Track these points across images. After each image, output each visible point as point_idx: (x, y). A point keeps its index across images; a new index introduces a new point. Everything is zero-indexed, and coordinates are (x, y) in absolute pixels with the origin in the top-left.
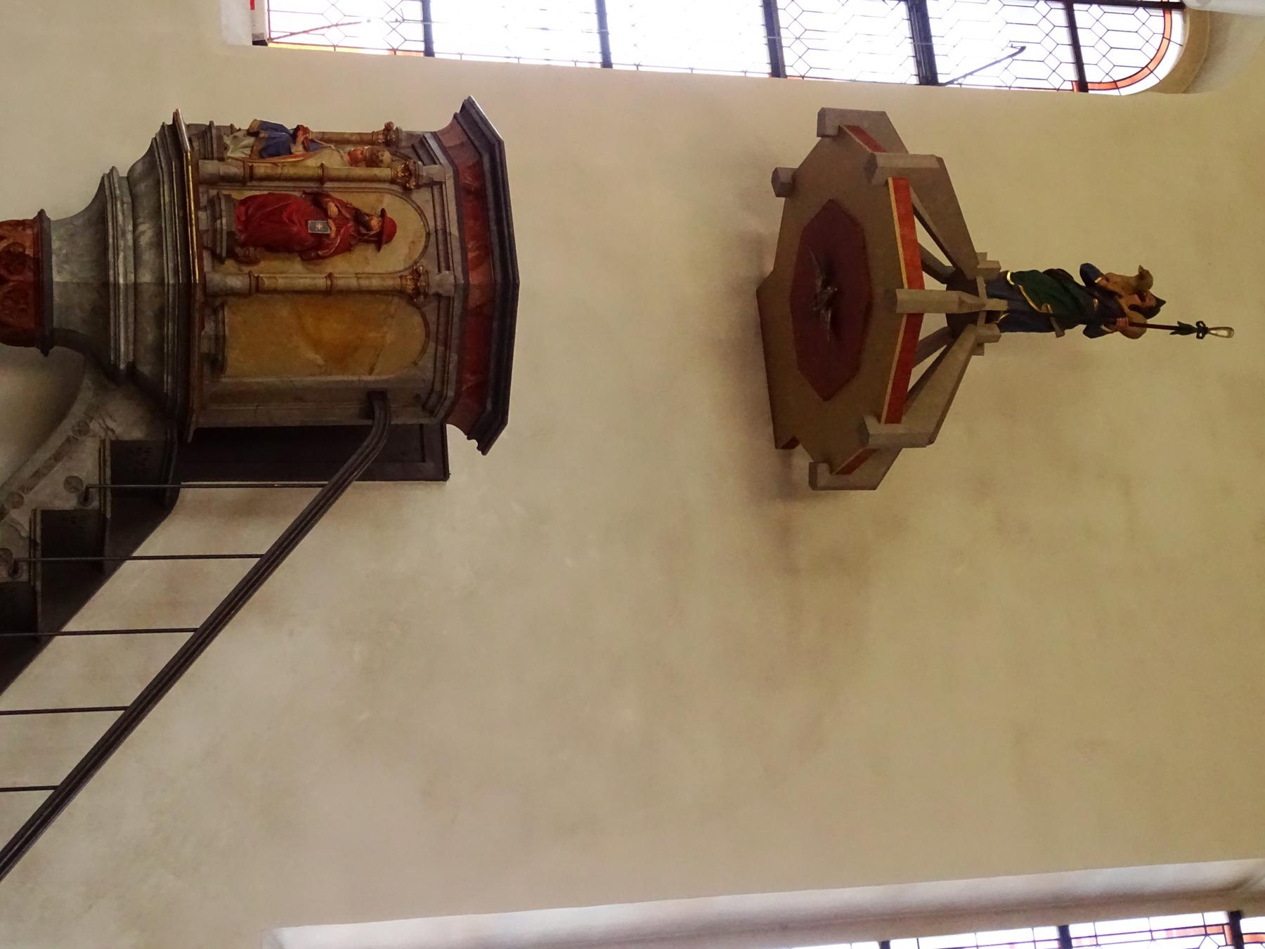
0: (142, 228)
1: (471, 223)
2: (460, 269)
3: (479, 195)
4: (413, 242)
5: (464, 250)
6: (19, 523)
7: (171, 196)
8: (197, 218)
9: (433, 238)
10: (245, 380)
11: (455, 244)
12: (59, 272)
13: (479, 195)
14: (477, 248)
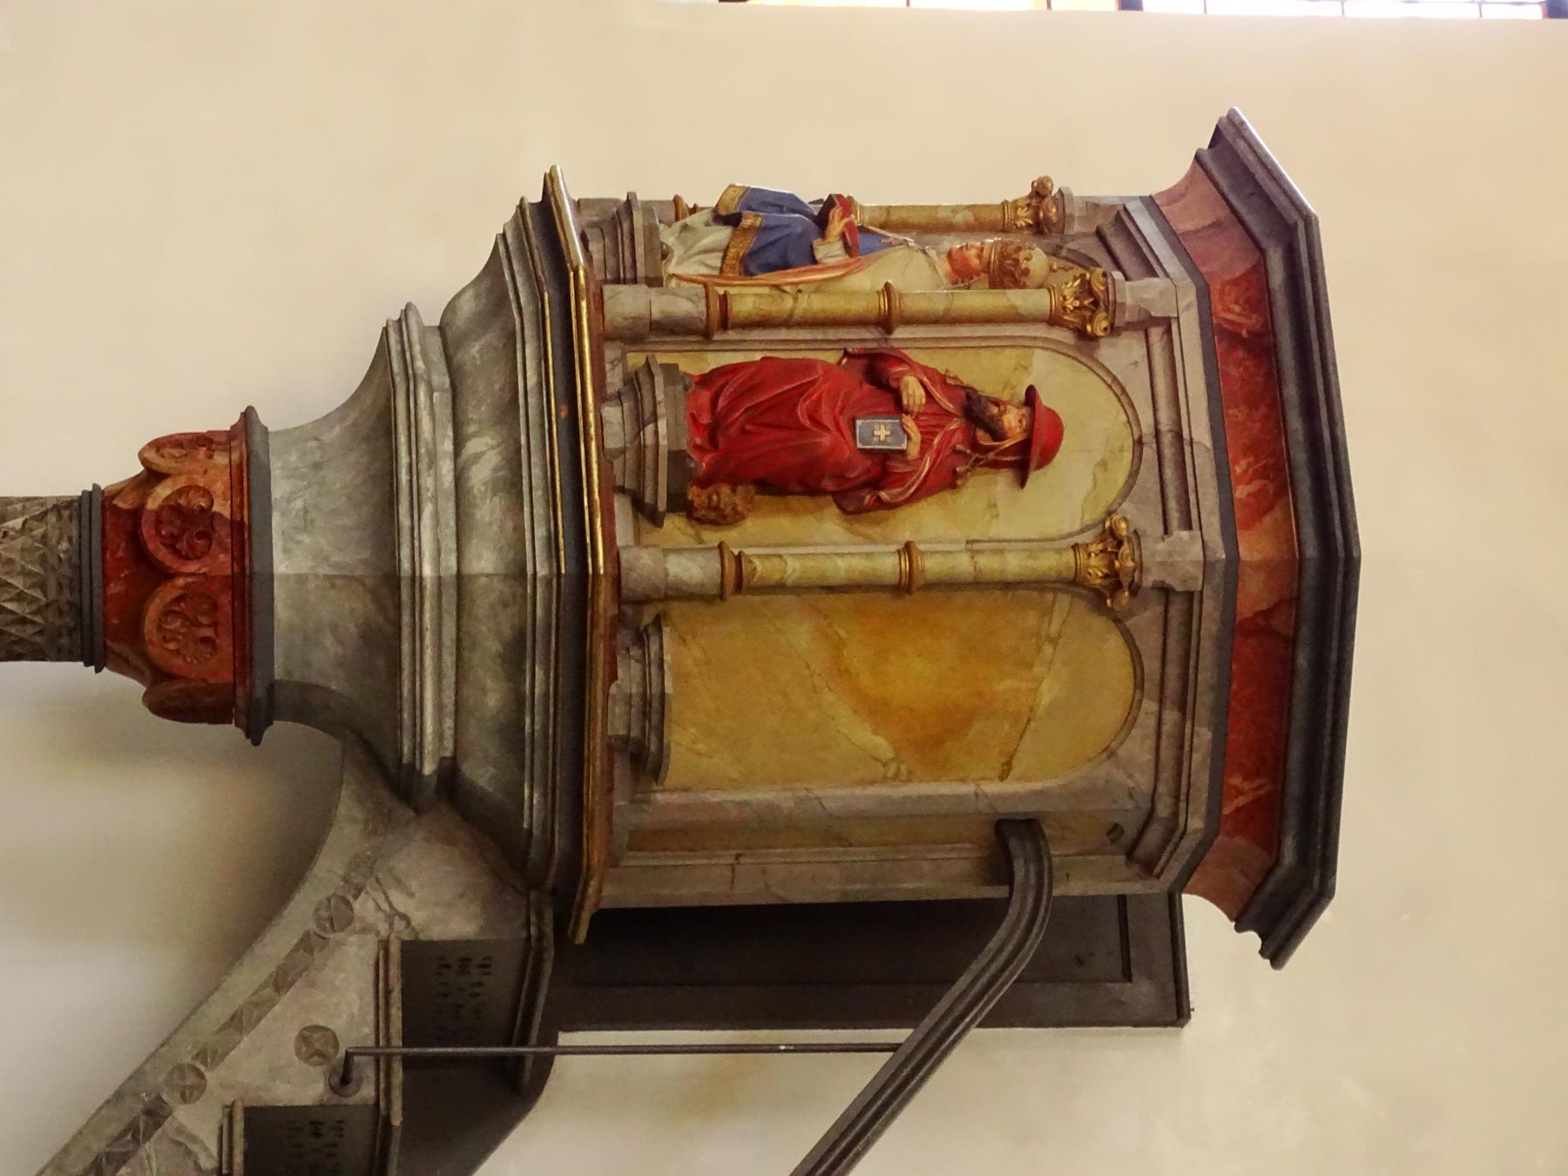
0: (472, 447)
3: (1261, 346)
4: (1103, 464)
6: (194, 1139)
9: (1149, 453)
11: (1203, 464)
13: (1261, 346)
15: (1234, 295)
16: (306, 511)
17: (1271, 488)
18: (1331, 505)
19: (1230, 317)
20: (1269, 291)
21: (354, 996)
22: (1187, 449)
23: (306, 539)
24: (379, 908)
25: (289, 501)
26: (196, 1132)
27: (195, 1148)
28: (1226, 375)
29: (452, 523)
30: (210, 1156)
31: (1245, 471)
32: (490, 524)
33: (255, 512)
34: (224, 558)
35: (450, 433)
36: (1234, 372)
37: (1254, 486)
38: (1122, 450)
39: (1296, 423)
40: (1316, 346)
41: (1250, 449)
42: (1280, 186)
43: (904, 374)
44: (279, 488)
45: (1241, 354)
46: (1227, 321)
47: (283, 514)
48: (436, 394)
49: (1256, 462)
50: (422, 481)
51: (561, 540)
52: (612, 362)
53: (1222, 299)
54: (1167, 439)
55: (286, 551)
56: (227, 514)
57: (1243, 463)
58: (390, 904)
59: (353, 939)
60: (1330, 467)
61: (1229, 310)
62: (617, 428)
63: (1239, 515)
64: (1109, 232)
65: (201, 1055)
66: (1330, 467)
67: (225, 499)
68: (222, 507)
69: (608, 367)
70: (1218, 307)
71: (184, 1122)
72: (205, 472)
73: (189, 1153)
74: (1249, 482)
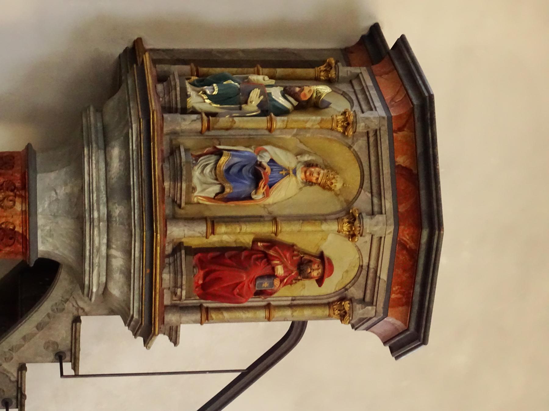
0: (113, 252)
1: (400, 271)
2: (382, 305)
3: (413, 254)
4: (347, 271)
5: (389, 291)
6: (8, 372)
7: (141, 251)
8: (161, 279)
9: (364, 272)
10: (219, 106)
11: (382, 287)
12: (43, 243)
13: (413, 254)
14: (400, 293)
15: (407, 232)
16: (50, 230)
17: (404, 300)
18: (426, 293)
19: (405, 239)
20: (420, 244)
21: (64, 332)
22: (378, 279)
23: (50, 240)
24: (73, 306)
25: (44, 226)
26: (9, 370)
27: (9, 375)
28: (398, 258)
29: (105, 267)
30: (14, 377)
31: (397, 290)
32: (119, 282)
33: (31, 236)
34: (20, 246)
35: (106, 236)
36: (401, 258)
37: (399, 296)
38: (354, 267)
39: (418, 289)
40: (431, 275)
41: (401, 284)
42: (423, 295)
43: (277, 265)
44: (41, 221)
45: (405, 252)
46: (403, 240)
47: (42, 230)
48: (101, 223)
49: (401, 288)
50: (94, 261)
51: (145, 240)
52: (168, 243)
53: (403, 232)
54: (372, 271)
55: (43, 243)
56: (21, 231)
57: (397, 287)
58: (78, 305)
59: (65, 315)
60: (425, 315)
61: (404, 236)
62: (167, 282)
63: (391, 303)
64: (371, 134)
65: (11, 350)
66: (425, 315)
67: (20, 226)
68: (18, 229)
69: (167, 245)
70: (400, 234)
71: (6, 368)
72: (12, 217)
73: (7, 376)
74: (397, 294)
